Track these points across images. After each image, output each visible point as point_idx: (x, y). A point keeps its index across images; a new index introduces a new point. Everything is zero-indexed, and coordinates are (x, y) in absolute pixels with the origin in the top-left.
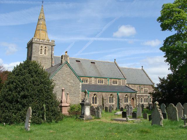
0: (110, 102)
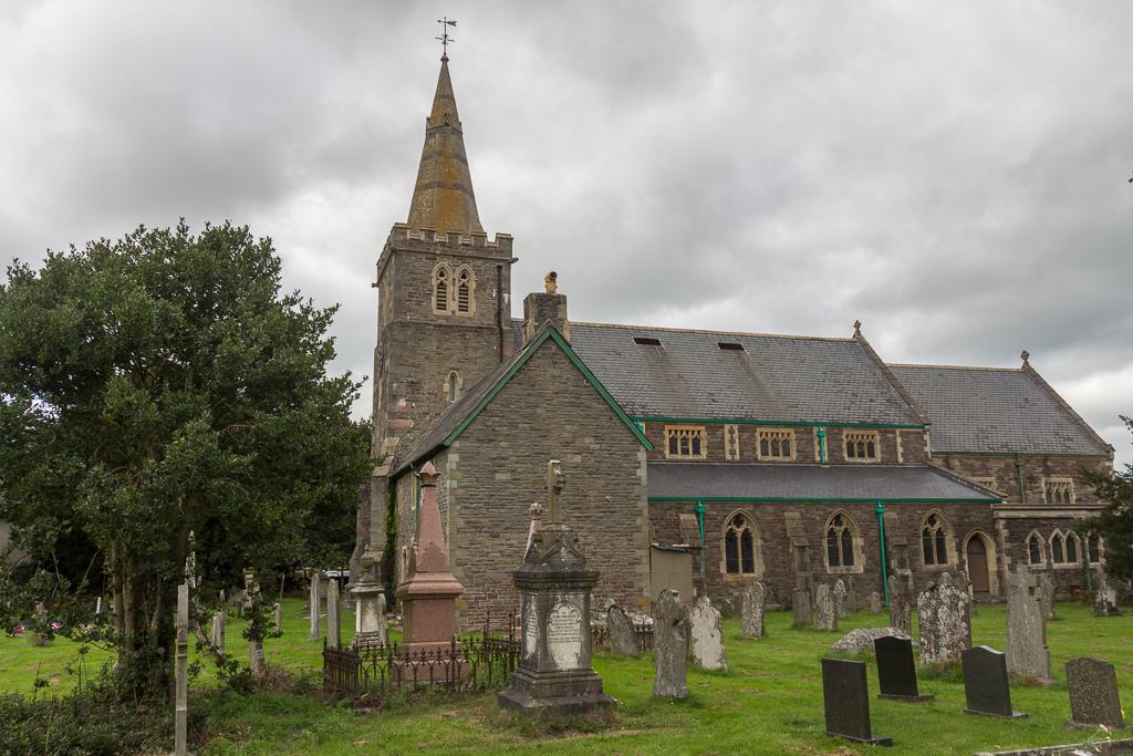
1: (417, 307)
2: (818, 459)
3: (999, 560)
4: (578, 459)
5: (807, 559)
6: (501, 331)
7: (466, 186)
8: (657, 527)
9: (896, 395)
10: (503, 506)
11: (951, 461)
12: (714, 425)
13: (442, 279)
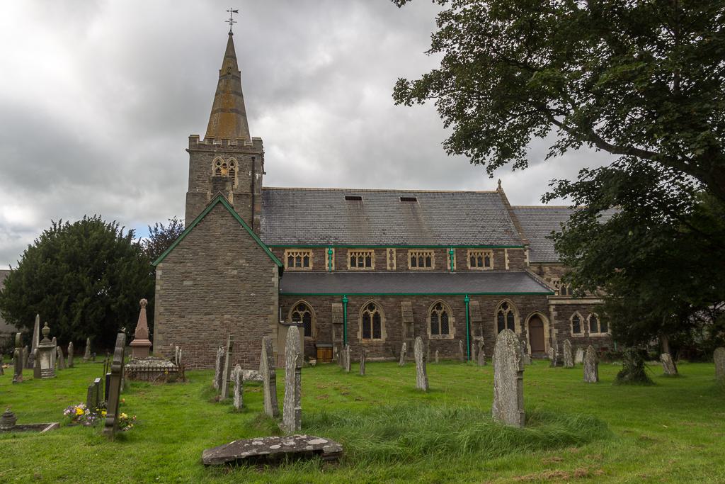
0: (435, 331)
1: (203, 184)
2: (449, 268)
3: (550, 331)
4: (235, 272)
5: (412, 330)
6: (253, 196)
7: (239, 109)
8: (317, 311)
9: (512, 226)
10: (187, 300)
11: (543, 268)
12: (380, 249)
13: (219, 166)
